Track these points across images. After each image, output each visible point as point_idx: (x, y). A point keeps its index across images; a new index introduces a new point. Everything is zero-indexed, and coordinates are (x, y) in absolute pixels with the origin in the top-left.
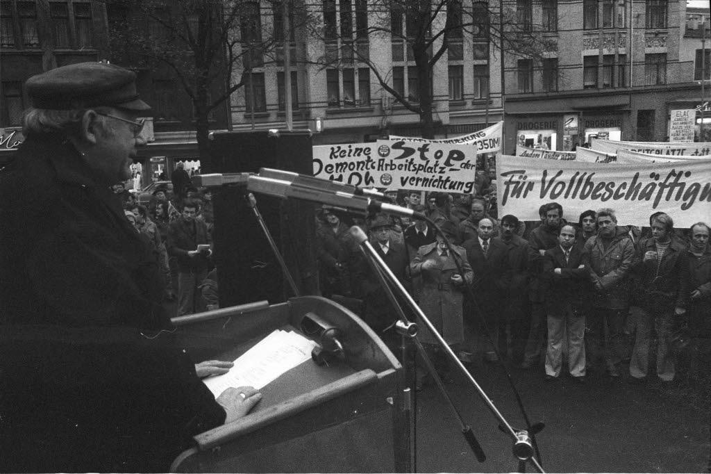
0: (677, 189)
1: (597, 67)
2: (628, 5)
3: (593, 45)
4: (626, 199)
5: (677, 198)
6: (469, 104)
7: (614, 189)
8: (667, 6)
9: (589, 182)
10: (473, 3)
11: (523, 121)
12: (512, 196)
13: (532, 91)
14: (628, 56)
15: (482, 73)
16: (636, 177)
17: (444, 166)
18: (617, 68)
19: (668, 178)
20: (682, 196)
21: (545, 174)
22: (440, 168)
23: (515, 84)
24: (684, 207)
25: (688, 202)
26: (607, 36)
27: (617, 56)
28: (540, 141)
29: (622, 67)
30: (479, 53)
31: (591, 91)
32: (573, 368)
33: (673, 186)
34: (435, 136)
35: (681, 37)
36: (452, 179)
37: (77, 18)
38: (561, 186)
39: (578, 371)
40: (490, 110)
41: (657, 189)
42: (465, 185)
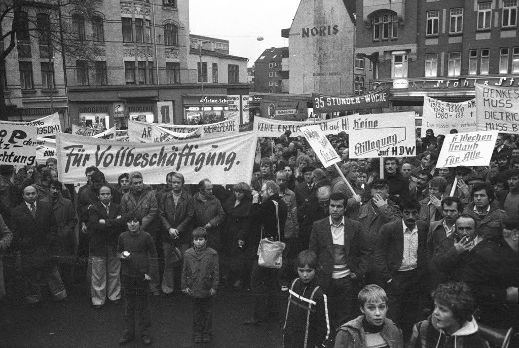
0: (191, 157)
2: (152, 27)
3: (131, 54)
4: (158, 165)
5: (192, 164)
6: (39, 93)
7: (149, 158)
8: (177, 31)
9: (130, 154)
10: (37, 14)
11: (82, 106)
12: (73, 165)
13: (89, 84)
14: (155, 63)
15: (48, 69)
16: (163, 150)
17: (8, 143)
18: (147, 71)
19: (184, 150)
20: (194, 162)
21: (98, 148)
22: (5, 145)
23: (74, 79)
24: (197, 170)
25: (199, 166)
26: (140, 48)
27: (147, 63)
28: (97, 121)
29: (152, 70)
31: (130, 86)
32: (111, 294)
33: (188, 155)
34: (9, 119)
35: (188, 53)
36: (15, 154)
38: (110, 157)
39: (114, 297)
40: (53, 98)
41: (178, 157)
42: (27, 159)
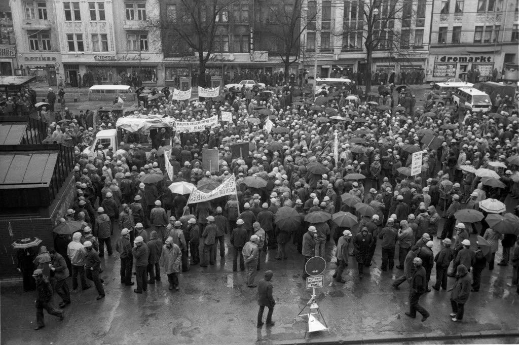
1: (482, 32)
30: (419, 24)
37: (339, 147)
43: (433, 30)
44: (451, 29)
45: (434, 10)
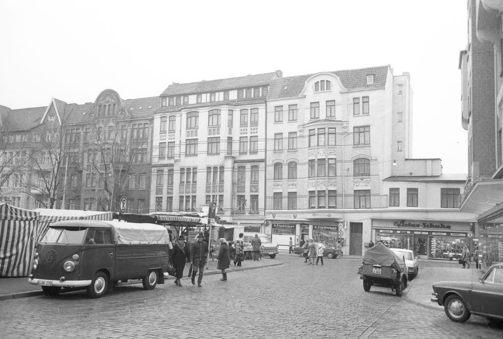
30: (253, 189)
43: (267, 195)
44: (285, 194)
45: (267, 176)
